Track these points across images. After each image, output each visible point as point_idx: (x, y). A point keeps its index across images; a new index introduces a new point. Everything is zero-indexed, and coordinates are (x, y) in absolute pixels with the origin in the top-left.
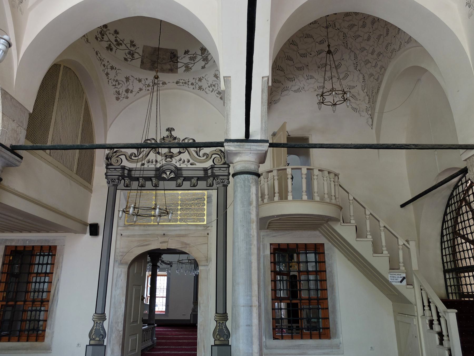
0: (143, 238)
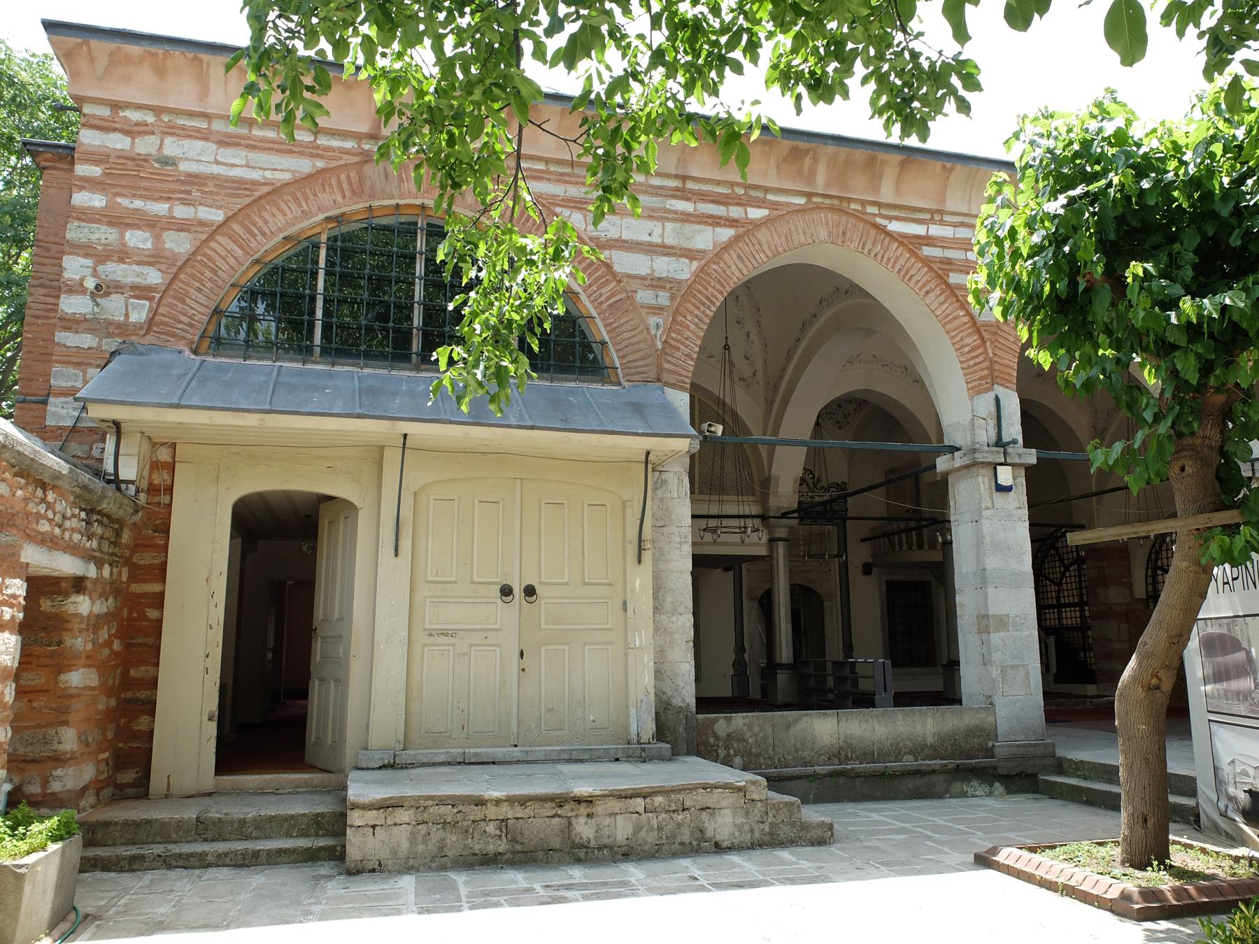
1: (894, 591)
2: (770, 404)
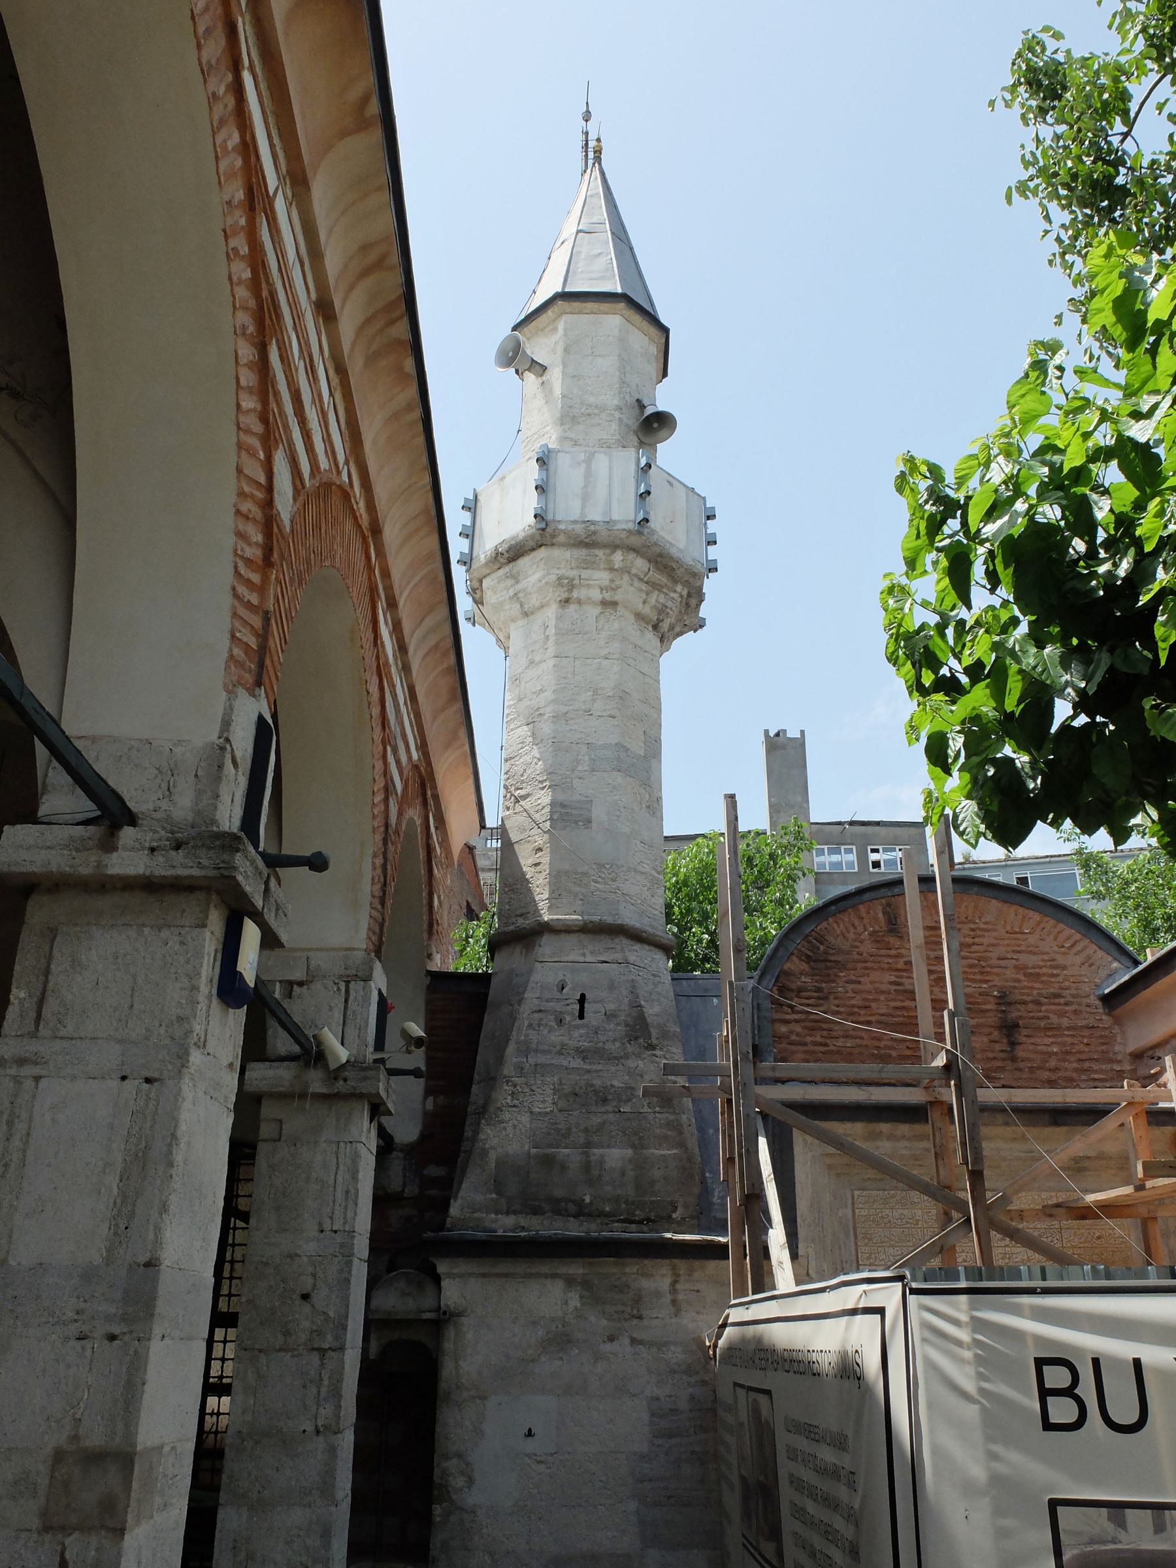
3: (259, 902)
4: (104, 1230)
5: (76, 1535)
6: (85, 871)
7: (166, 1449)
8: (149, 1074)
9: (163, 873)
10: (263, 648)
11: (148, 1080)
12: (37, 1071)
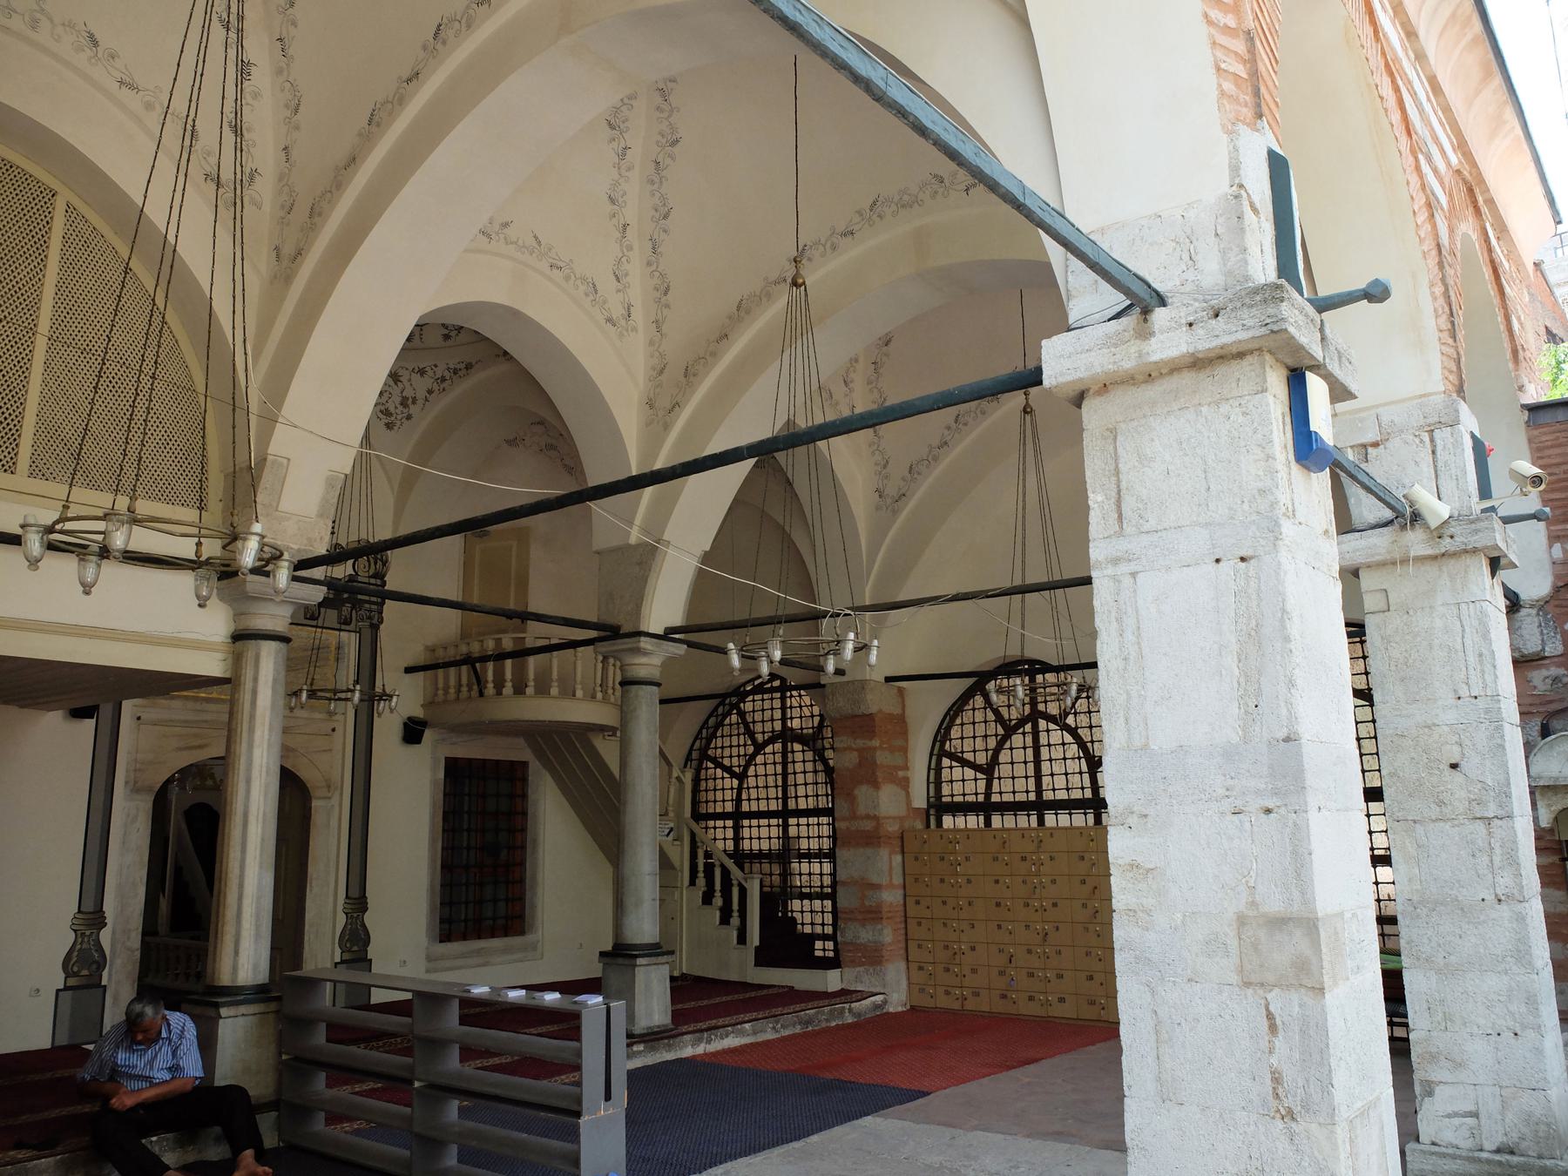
0: (194, 730)
1: (459, 776)
2: (287, 260)
3: (1317, 352)
4: (1234, 710)
5: (1276, 990)
6: (1128, 364)
7: (1348, 915)
8: (1244, 554)
9: (1208, 345)
10: (1255, 74)
11: (1243, 559)
12: (1133, 567)
